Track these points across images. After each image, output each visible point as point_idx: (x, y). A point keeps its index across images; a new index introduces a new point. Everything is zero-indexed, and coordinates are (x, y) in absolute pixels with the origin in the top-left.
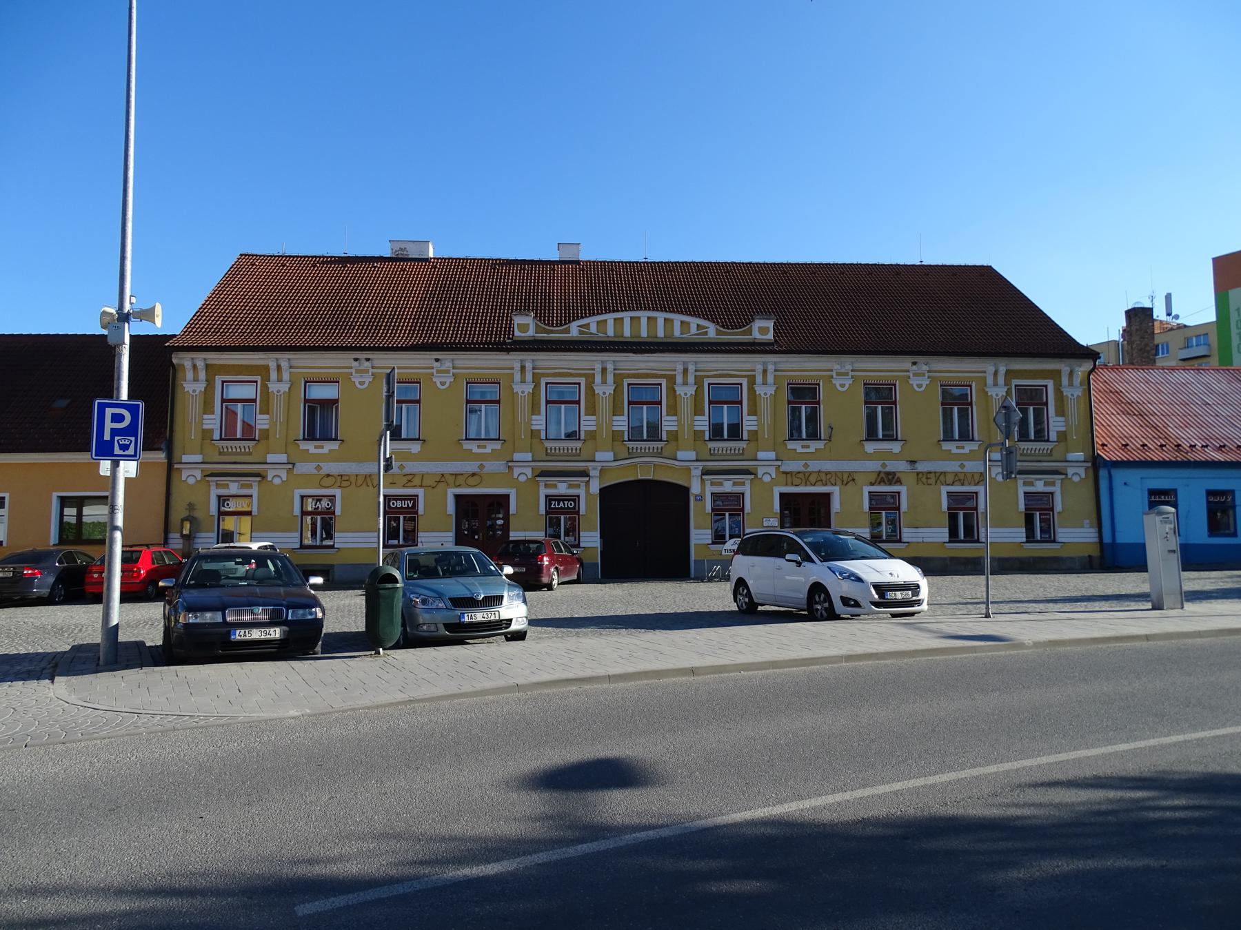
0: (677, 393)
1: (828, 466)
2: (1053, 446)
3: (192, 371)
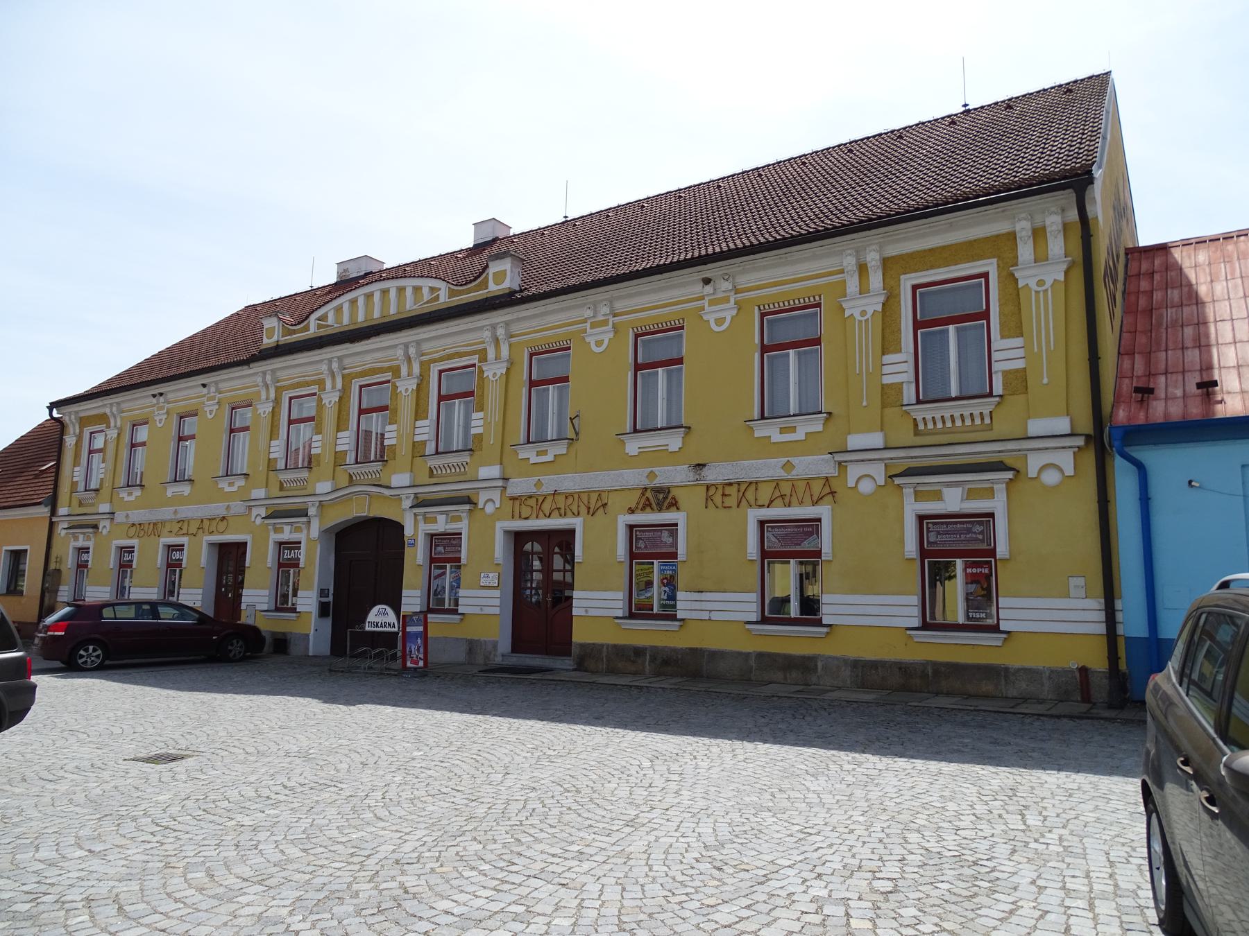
0: (1020, 285)
1: (569, 482)
2: (992, 408)
3: (856, 277)
